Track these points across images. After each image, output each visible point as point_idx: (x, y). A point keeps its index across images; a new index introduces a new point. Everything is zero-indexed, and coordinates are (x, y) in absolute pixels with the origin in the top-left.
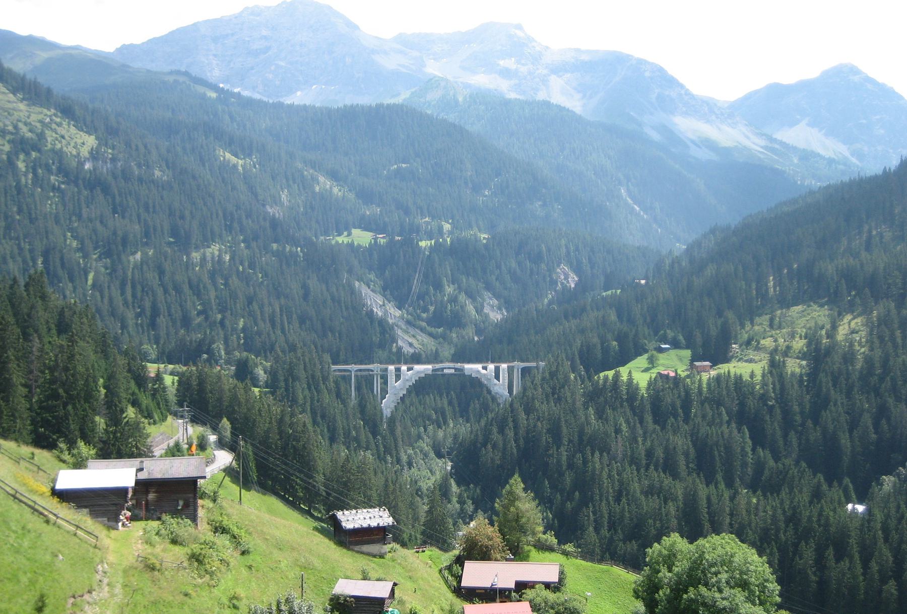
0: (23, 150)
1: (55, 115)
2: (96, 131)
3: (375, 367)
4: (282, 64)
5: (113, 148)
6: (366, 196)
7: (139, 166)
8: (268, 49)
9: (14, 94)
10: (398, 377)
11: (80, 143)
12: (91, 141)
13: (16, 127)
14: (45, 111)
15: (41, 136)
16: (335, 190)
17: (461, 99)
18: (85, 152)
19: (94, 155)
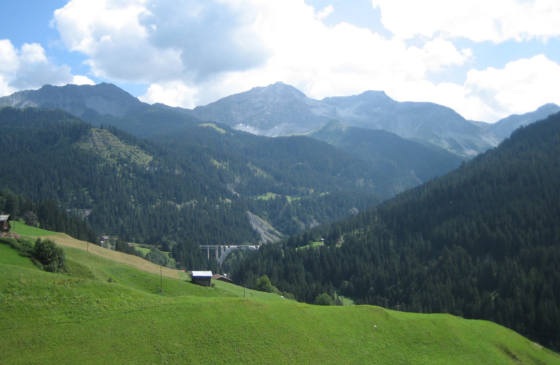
0: (121, 163)
1: (137, 148)
2: (153, 154)
3: (217, 246)
4: (268, 113)
5: (159, 161)
6: (278, 178)
7: (170, 168)
8: (263, 107)
9: (121, 141)
10: (224, 251)
11: (144, 159)
12: (150, 158)
13: (119, 154)
14: (133, 147)
15: (129, 157)
16: (265, 175)
17: (343, 130)
18: (147, 163)
19: (151, 164)
